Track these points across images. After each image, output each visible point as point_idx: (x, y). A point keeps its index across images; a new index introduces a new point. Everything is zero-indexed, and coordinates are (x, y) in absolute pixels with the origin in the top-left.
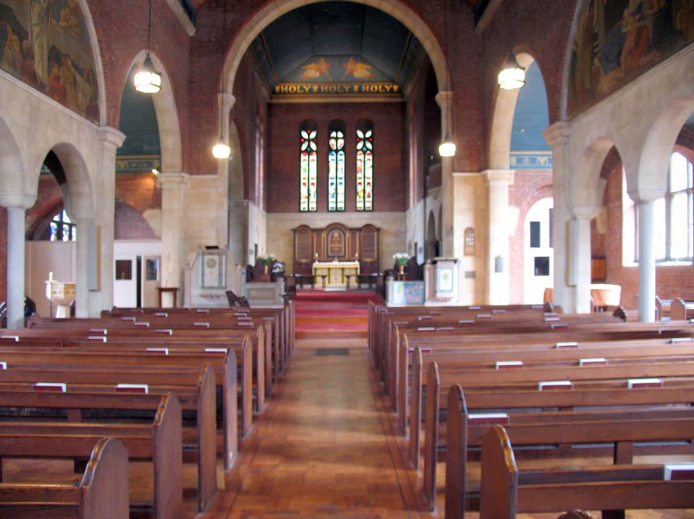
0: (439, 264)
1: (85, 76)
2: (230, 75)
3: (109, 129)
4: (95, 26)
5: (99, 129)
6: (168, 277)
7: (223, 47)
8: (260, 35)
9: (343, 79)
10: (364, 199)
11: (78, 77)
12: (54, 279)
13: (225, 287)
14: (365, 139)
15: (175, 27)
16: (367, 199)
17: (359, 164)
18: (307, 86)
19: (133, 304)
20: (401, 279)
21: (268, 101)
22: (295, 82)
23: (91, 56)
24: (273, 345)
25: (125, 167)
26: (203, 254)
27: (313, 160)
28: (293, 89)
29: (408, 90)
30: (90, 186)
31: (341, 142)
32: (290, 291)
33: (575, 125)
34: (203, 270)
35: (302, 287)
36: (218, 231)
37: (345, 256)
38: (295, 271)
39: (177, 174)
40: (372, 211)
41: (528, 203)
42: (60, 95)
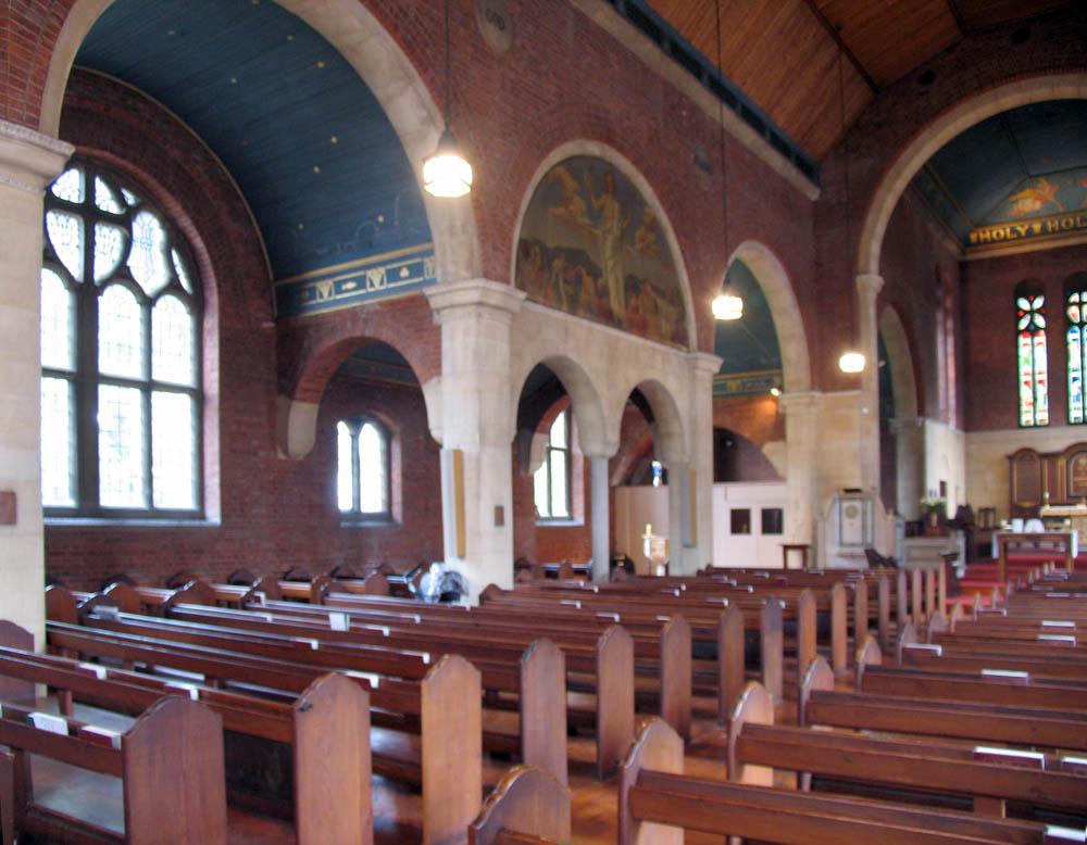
2: (872, 247)
3: (701, 355)
6: (794, 530)
8: (925, 167)
11: (660, 302)
12: (653, 532)
15: (786, 197)
18: (1022, 226)
22: (1002, 223)
25: (738, 388)
26: (841, 500)
27: (1040, 343)
28: (998, 234)
30: (681, 425)
36: (863, 468)
42: (640, 327)
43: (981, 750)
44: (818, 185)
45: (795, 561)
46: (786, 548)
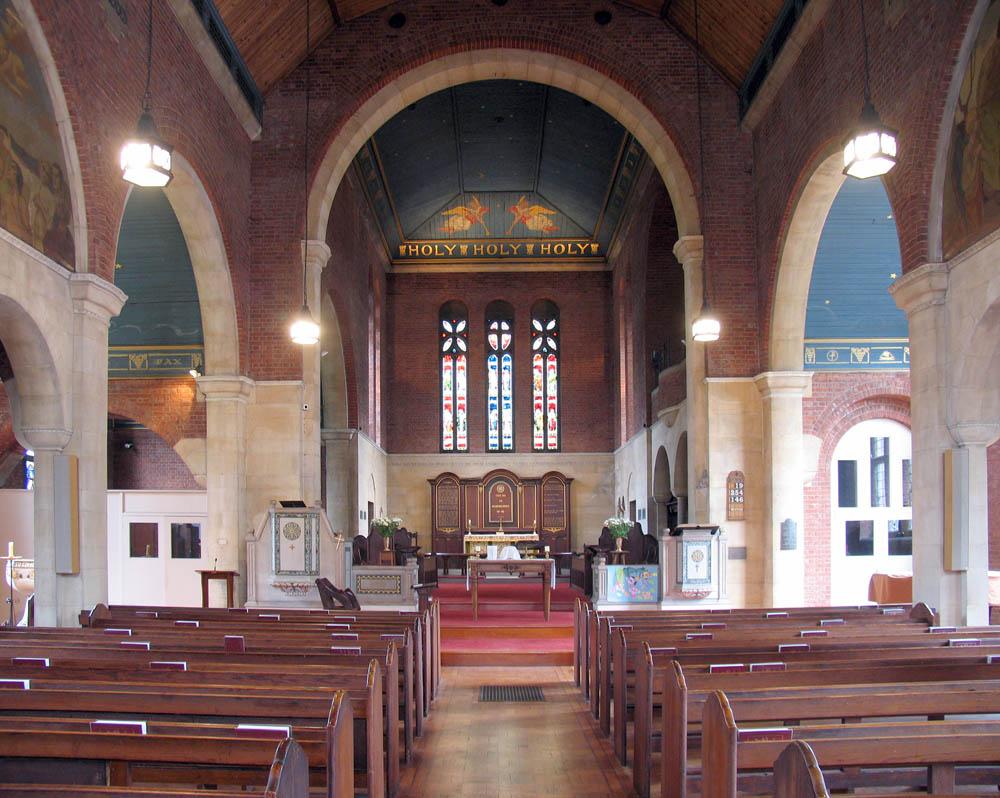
0: (686, 535)
1: (43, 174)
2: (321, 209)
3: (91, 277)
4: (63, 82)
5: (74, 277)
6: (216, 551)
7: (308, 159)
9: (509, 233)
10: (545, 426)
11: (26, 173)
13: (317, 573)
14: (546, 334)
15: (221, 115)
16: (550, 432)
17: (538, 375)
19: (199, 604)
20: (620, 562)
21: (388, 271)
23: (55, 138)
24: (402, 686)
25: (143, 365)
26: (278, 516)
27: (462, 368)
29: (616, 250)
30: (56, 383)
31: (506, 338)
32: (428, 581)
33: (961, 267)
34: (278, 541)
35: (446, 573)
37: (514, 523)
38: (435, 548)
39: (233, 379)
40: (558, 450)
41: (836, 429)
43: (241, 727)
44: (261, 123)
45: (218, 598)
46: (207, 576)
